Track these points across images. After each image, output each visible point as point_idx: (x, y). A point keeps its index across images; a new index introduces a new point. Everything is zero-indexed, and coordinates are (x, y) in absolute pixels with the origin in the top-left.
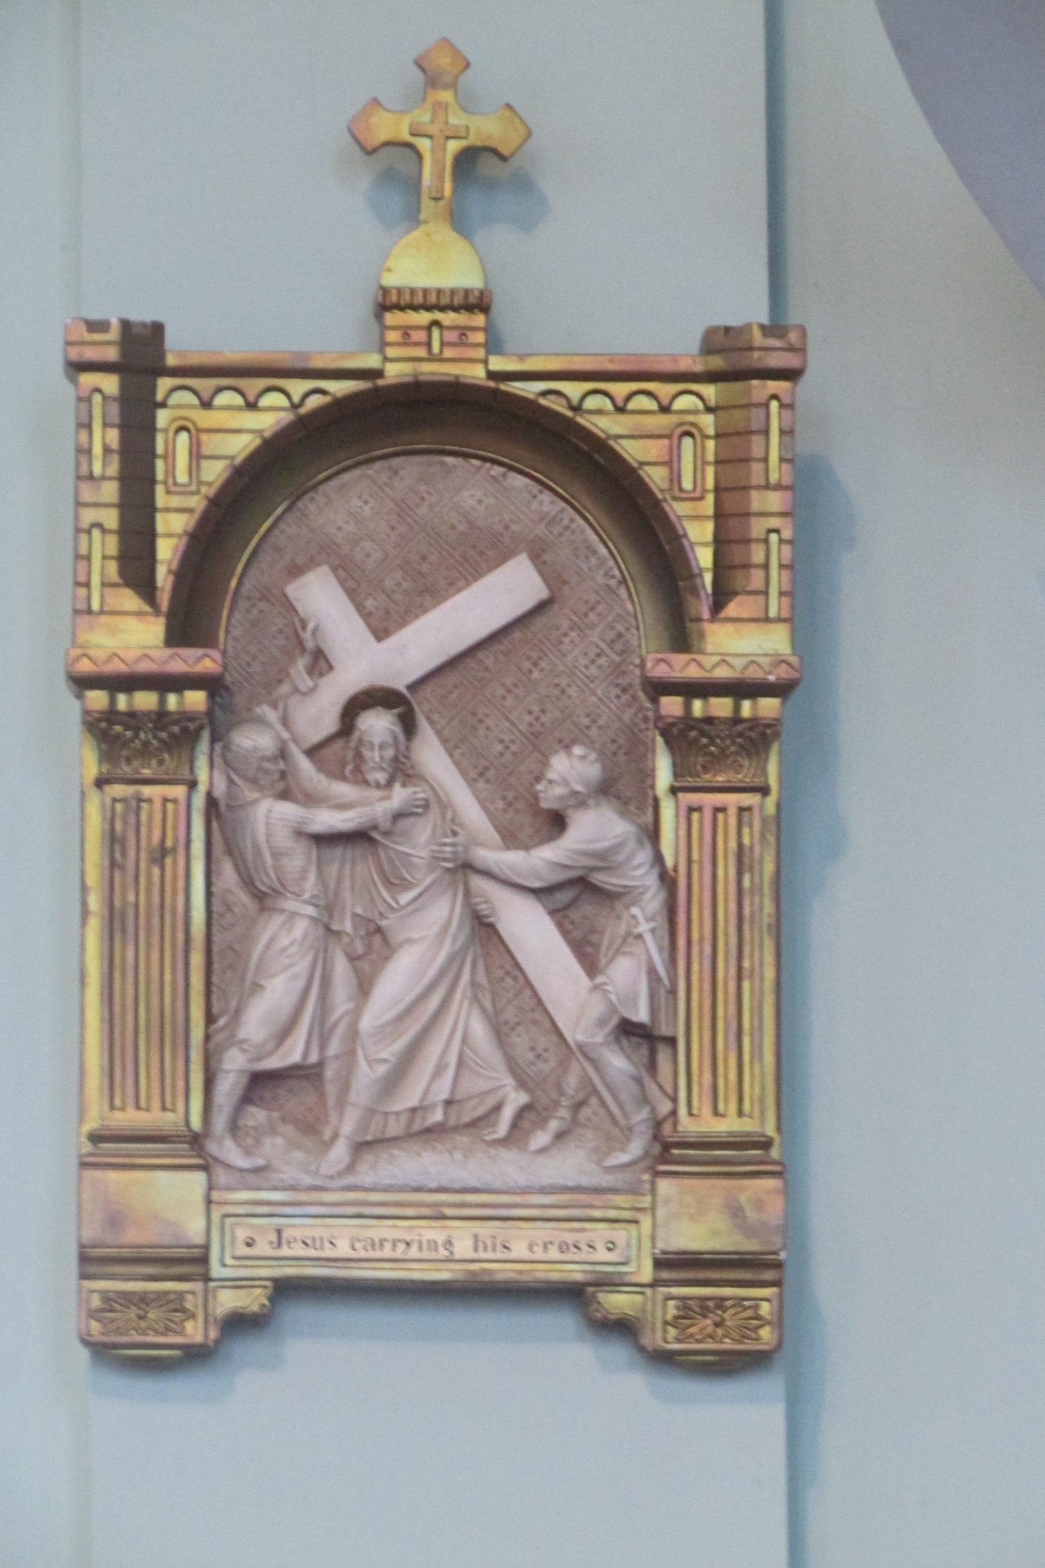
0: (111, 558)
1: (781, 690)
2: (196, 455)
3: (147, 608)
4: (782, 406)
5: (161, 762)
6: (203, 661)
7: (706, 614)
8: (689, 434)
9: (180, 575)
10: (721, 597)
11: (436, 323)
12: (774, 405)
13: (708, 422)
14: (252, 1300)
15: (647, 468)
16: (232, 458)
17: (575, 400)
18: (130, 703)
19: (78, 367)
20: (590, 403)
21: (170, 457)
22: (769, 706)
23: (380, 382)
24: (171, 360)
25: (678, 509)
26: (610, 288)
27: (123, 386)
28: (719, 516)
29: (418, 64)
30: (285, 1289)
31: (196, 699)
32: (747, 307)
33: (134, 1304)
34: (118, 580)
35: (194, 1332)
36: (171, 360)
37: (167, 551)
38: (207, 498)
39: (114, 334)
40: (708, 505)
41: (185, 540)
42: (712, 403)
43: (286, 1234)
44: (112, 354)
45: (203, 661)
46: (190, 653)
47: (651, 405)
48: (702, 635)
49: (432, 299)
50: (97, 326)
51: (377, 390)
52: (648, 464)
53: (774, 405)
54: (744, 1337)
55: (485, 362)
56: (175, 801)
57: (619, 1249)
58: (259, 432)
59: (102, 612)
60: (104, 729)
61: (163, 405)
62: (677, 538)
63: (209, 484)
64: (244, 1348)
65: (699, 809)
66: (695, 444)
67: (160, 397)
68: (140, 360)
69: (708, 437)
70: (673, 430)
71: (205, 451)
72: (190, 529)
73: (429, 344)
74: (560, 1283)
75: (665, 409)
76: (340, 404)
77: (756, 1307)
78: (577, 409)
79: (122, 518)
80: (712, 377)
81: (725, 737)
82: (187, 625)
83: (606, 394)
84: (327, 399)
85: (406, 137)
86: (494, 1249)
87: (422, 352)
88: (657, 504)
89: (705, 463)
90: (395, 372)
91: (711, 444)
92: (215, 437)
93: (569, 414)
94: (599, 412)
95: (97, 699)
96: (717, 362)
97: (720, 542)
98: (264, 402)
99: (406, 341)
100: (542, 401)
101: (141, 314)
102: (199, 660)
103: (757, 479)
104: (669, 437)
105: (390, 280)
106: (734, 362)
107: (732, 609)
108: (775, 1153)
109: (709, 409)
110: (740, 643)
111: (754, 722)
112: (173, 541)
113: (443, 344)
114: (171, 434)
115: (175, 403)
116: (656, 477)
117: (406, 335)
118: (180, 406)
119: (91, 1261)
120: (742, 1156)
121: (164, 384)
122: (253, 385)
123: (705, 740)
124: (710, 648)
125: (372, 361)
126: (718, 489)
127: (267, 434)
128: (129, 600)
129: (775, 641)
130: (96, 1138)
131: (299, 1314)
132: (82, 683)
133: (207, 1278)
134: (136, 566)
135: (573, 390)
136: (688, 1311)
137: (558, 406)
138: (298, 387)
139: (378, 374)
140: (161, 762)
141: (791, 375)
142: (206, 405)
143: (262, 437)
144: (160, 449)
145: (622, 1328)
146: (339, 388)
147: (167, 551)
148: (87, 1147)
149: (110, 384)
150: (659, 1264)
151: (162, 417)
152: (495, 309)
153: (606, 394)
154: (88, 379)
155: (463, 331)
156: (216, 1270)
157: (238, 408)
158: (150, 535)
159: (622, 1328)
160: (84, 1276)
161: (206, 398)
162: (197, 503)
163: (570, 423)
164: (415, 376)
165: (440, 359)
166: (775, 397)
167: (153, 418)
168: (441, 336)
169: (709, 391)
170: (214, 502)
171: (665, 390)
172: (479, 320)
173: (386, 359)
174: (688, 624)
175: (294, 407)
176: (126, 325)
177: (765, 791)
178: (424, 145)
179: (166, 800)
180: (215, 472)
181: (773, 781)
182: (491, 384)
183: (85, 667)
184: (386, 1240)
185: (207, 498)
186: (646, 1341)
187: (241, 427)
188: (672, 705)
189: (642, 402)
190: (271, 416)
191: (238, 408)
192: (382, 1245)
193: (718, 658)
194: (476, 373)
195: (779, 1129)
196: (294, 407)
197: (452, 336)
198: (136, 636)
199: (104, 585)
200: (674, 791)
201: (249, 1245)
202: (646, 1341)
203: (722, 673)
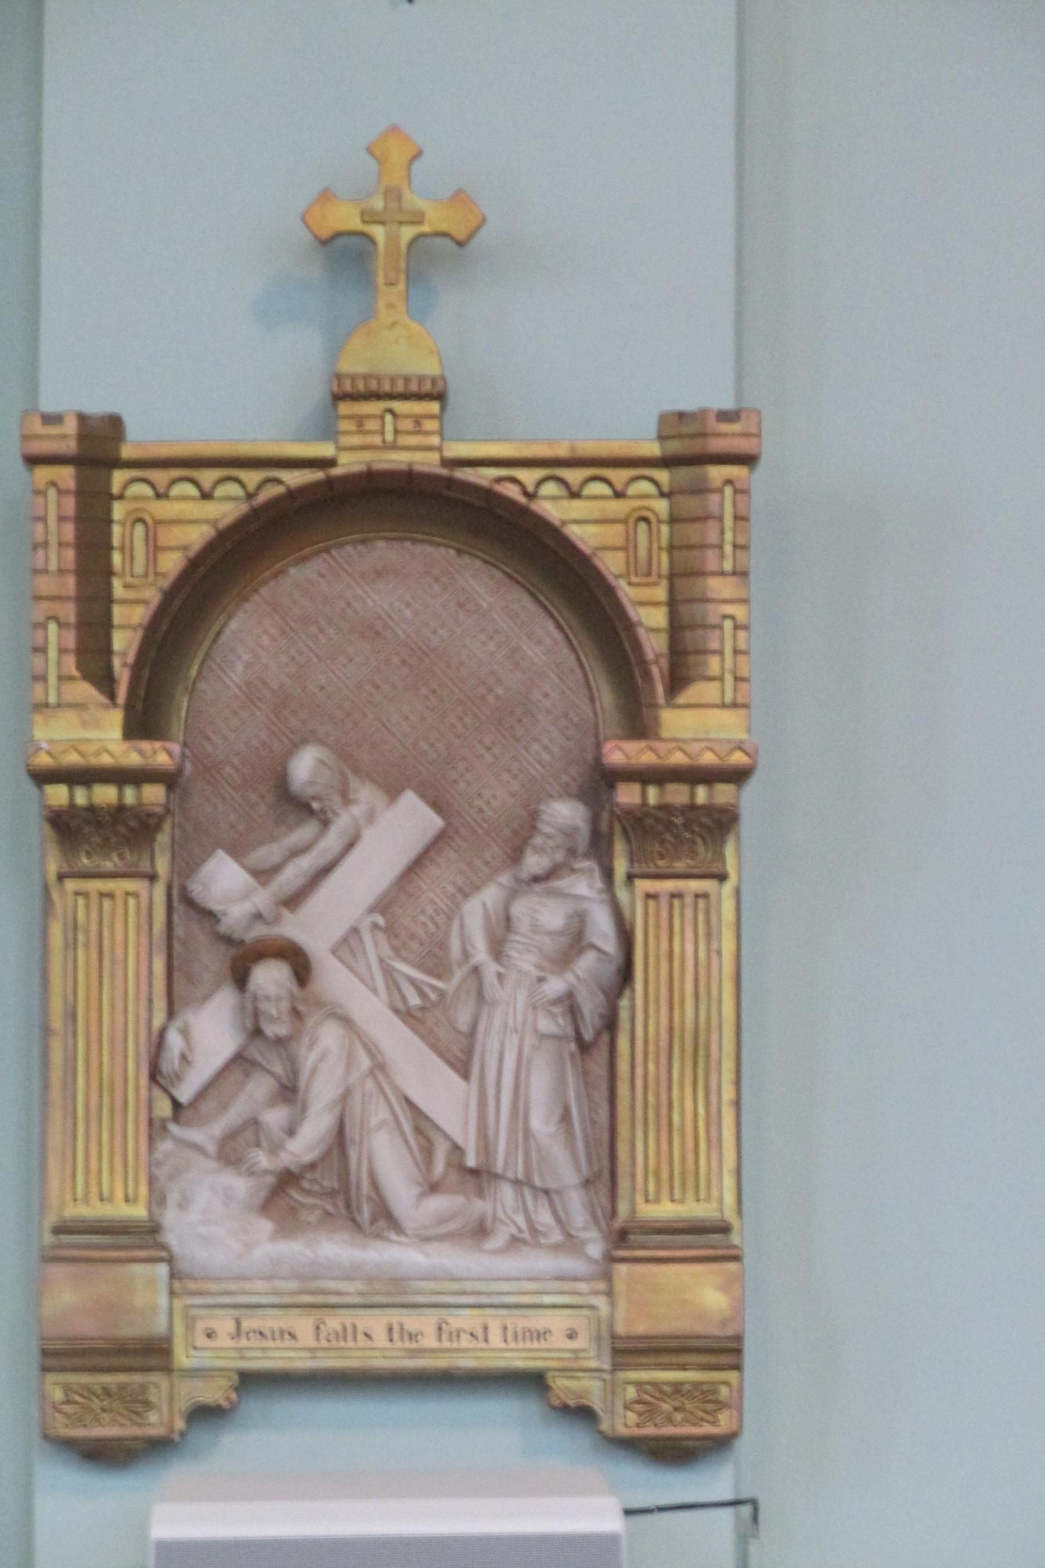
0: (714, 652)
1: (739, 776)
2: (154, 549)
3: (104, 699)
4: (736, 491)
5: (693, 854)
6: (160, 755)
7: (661, 699)
8: (646, 520)
9: (137, 668)
10: (678, 679)
11: (391, 411)
12: (728, 491)
13: (662, 506)
14: (213, 1393)
15: (600, 554)
16: (185, 548)
17: (530, 489)
18: (139, 797)
19: (33, 461)
20: (550, 489)
21: (127, 550)
22: (724, 793)
23: (336, 471)
24: (127, 452)
25: (627, 592)
26: (546, 382)
27: (80, 479)
28: (673, 604)
29: (370, 150)
30: (251, 1381)
31: (154, 794)
32: (707, 391)
33: (669, 1396)
34: (75, 673)
35: (154, 1424)
36: (127, 452)
37: (124, 642)
38: (161, 590)
39: (71, 427)
40: (661, 593)
41: (140, 634)
42: (666, 489)
43: (246, 1325)
44: (70, 446)
45: (160, 755)
46: (146, 745)
47: (191, 490)
48: (657, 721)
49: (414, 387)
50: (52, 419)
51: (330, 482)
52: (605, 548)
53: (728, 491)
54: (702, 1420)
55: (440, 449)
56: (136, 895)
57: (560, 1336)
58: (214, 523)
59: (59, 705)
60: (66, 826)
61: (121, 497)
62: (630, 626)
63: (164, 575)
64: (200, 1436)
65: (111, 896)
66: (650, 530)
67: (116, 489)
68: (97, 451)
69: (659, 521)
70: (629, 515)
71: (161, 543)
72: (146, 620)
73: (382, 433)
74: (470, 1369)
75: (619, 495)
76: (292, 494)
77: (715, 1392)
78: (531, 496)
79: (79, 614)
80: (666, 462)
81: (674, 827)
82: (142, 723)
83: (608, 482)
84: (279, 490)
85: (356, 224)
86: (282, 1339)
87: (377, 440)
88: (610, 591)
89: (122, 549)
90: (349, 463)
91: (665, 529)
92: (170, 527)
93: (522, 500)
94: (554, 498)
95: (58, 794)
96: (675, 447)
97: (676, 628)
98: (632, 490)
99: (361, 430)
100: (499, 488)
101: (97, 406)
102: (641, 751)
103: (712, 565)
104: (624, 521)
105: (347, 366)
106: (695, 453)
107: (698, 691)
108: (735, 1239)
109: (662, 495)
110: (694, 727)
111: (709, 809)
112: (129, 634)
113: (396, 432)
114: (128, 524)
115: (130, 493)
116: (611, 564)
117: (360, 424)
118: (137, 498)
119: (60, 1355)
120: (706, 1240)
121: (119, 477)
122: (208, 477)
123: (660, 827)
124: (665, 733)
125: (326, 450)
126: (672, 576)
127: (223, 524)
128: (85, 691)
129: (727, 726)
130: (57, 1231)
131: (254, 1406)
132: (43, 777)
133: (167, 1369)
134: (93, 659)
135: (528, 476)
136: (647, 1403)
137: (512, 492)
138: (252, 477)
139: (331, 463)
140: (121, 857)
141: (748, 460)
142: (160, 496)
143: (217, 529)
144: (116, 541)
145: (582, 1414)
146: (294, 478)
147: (124, 642)
148: (48, 1238)
149: (66, 475)
150: (616, 1352)
151: (118, 510)
152: (452, 397)
153: (513, 480)
154: (44, 474)
155: (418, 420)
156: (182, 1358)
157: (193, 498)
158: (106, 625)
159: (582, 1414)
160: (726, 1351)
161: (575, 488)
162: (153, 596)
163: (525, 512)
164: (410, 464)
165: (394, 447)
166: (729, 482)
167: (109, 511)
168: (395, 424)
169: (663, 476)
170: (169, 596)
171: (619, 476)
172: (434, 407)
173: (339, 449)
174: (644, 710)
175: (250, 496)
176: (82, 418)
177: (722, 877)
178: (378, 232)
179: (127, 894)
180: (172, 563)
181: (162, 866)
182: (444, 472)
183: (44, 760)
184: (463, 1330)
185: (161, 590)
186: (605, 1426)
187: (195, 517)
188: (628, 795)
189: (598, 488)
190: (226, 507)
191: (193, 498)
192: (458, 1336)
193: (704, 744)
194: (427, 462)
195: (739, 1211)
196: (250, 496)
197: (408, 425)
198: (100, 734)
199: (61, 678)
200: (630, 878)
201: (209, 1336)
202: (605, 1426)
203: (678, 759)
